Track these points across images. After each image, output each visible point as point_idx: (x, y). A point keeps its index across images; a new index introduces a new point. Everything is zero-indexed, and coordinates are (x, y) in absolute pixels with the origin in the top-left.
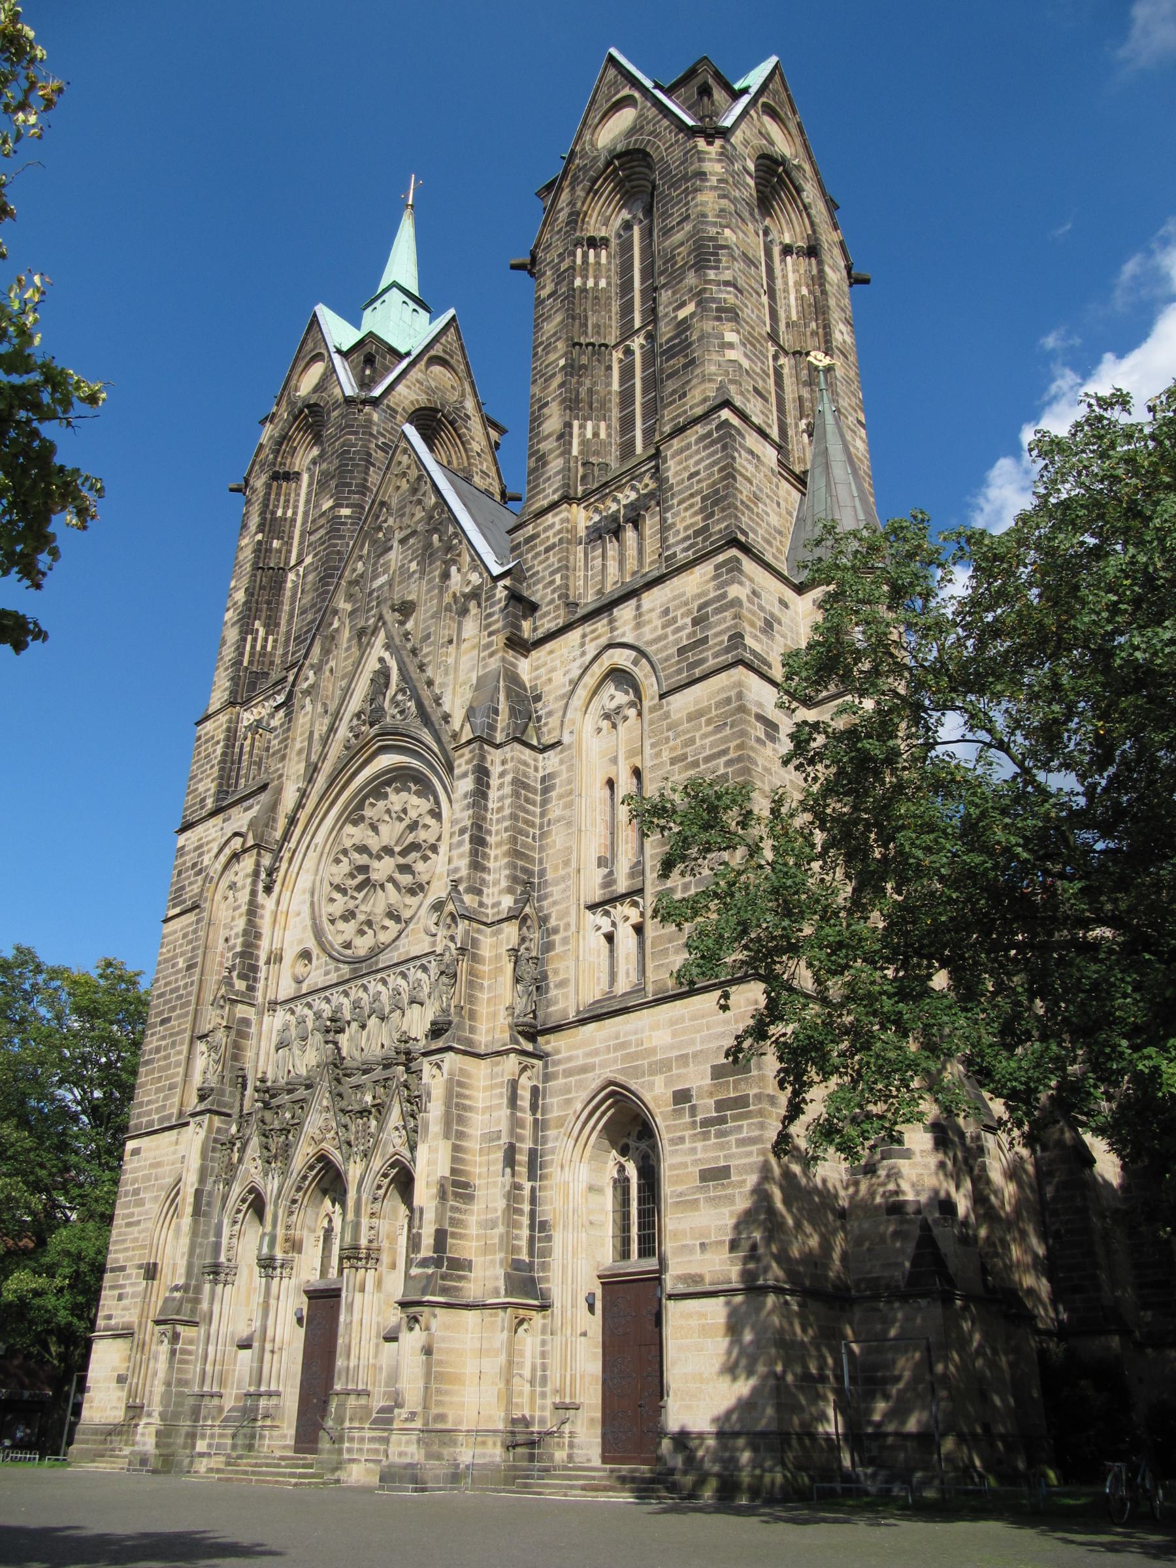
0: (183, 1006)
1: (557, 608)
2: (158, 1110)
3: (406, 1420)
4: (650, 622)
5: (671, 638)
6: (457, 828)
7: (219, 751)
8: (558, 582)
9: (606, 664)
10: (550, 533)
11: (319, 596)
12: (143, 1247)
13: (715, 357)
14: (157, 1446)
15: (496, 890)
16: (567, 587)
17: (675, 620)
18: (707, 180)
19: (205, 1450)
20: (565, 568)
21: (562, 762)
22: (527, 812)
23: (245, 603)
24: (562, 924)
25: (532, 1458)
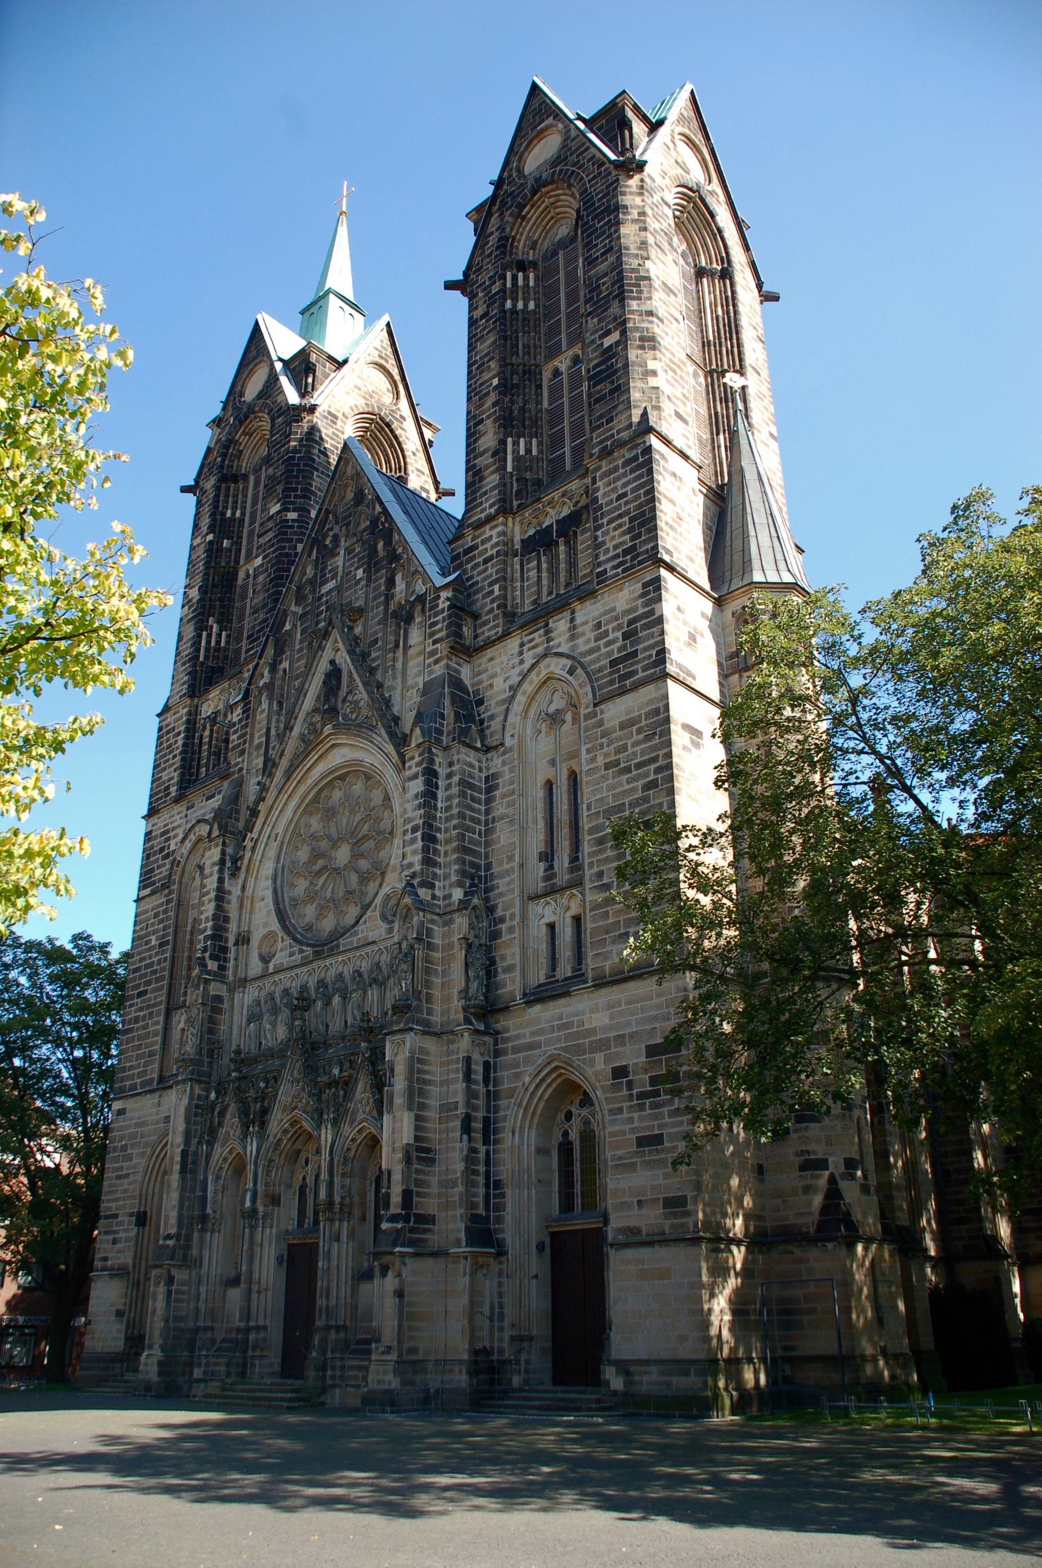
0: (157, 980)
1: (496, 617)
2: (139, 1075)
3: (383, 1353)
4: (583, 634)
5: (603, 650)
6: (409, 826)
7: (180, 743)
8: (497, 593)
9: (544, 673)
10: (488, 545)
11: (269, 596)
12: (133, 1197)
13: (639, 384)
14: (160, 1374)
15: (447, 883)
16: (505, 597)
17: (606, 633)
18: (628, 213)
19: (201, 1376)
20: (503, 579)
21: (504, 763)
22: (473, 810)
23: (199, 601)
24: (507, 914)
25: (492, 1382)
